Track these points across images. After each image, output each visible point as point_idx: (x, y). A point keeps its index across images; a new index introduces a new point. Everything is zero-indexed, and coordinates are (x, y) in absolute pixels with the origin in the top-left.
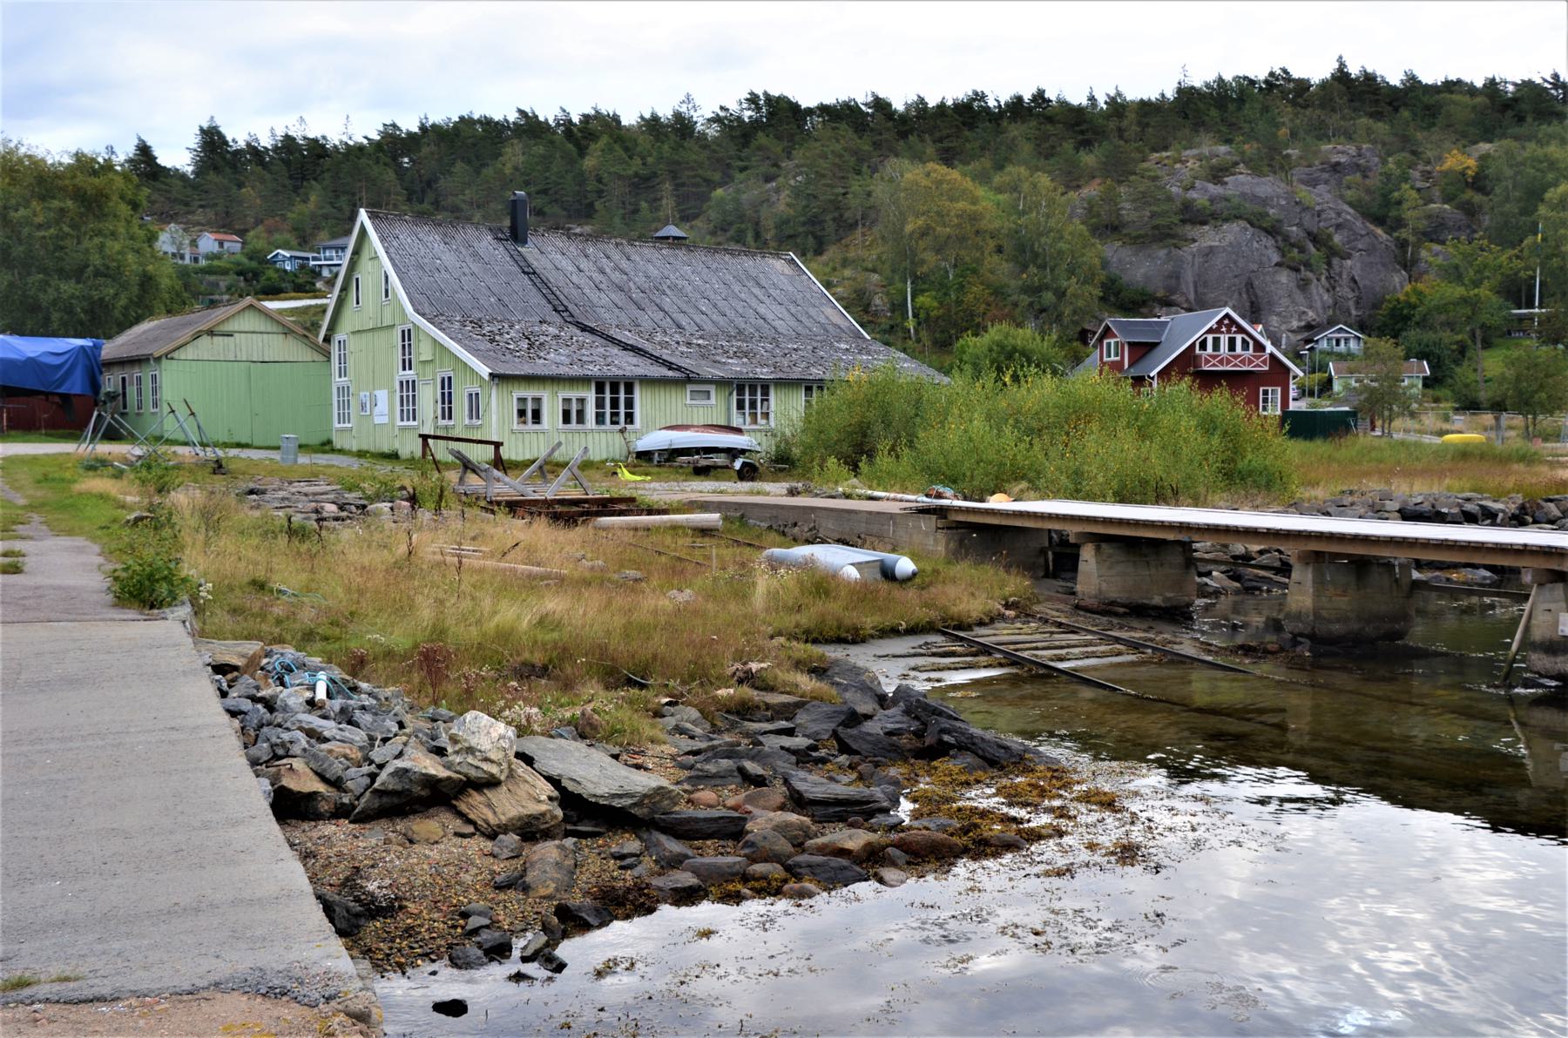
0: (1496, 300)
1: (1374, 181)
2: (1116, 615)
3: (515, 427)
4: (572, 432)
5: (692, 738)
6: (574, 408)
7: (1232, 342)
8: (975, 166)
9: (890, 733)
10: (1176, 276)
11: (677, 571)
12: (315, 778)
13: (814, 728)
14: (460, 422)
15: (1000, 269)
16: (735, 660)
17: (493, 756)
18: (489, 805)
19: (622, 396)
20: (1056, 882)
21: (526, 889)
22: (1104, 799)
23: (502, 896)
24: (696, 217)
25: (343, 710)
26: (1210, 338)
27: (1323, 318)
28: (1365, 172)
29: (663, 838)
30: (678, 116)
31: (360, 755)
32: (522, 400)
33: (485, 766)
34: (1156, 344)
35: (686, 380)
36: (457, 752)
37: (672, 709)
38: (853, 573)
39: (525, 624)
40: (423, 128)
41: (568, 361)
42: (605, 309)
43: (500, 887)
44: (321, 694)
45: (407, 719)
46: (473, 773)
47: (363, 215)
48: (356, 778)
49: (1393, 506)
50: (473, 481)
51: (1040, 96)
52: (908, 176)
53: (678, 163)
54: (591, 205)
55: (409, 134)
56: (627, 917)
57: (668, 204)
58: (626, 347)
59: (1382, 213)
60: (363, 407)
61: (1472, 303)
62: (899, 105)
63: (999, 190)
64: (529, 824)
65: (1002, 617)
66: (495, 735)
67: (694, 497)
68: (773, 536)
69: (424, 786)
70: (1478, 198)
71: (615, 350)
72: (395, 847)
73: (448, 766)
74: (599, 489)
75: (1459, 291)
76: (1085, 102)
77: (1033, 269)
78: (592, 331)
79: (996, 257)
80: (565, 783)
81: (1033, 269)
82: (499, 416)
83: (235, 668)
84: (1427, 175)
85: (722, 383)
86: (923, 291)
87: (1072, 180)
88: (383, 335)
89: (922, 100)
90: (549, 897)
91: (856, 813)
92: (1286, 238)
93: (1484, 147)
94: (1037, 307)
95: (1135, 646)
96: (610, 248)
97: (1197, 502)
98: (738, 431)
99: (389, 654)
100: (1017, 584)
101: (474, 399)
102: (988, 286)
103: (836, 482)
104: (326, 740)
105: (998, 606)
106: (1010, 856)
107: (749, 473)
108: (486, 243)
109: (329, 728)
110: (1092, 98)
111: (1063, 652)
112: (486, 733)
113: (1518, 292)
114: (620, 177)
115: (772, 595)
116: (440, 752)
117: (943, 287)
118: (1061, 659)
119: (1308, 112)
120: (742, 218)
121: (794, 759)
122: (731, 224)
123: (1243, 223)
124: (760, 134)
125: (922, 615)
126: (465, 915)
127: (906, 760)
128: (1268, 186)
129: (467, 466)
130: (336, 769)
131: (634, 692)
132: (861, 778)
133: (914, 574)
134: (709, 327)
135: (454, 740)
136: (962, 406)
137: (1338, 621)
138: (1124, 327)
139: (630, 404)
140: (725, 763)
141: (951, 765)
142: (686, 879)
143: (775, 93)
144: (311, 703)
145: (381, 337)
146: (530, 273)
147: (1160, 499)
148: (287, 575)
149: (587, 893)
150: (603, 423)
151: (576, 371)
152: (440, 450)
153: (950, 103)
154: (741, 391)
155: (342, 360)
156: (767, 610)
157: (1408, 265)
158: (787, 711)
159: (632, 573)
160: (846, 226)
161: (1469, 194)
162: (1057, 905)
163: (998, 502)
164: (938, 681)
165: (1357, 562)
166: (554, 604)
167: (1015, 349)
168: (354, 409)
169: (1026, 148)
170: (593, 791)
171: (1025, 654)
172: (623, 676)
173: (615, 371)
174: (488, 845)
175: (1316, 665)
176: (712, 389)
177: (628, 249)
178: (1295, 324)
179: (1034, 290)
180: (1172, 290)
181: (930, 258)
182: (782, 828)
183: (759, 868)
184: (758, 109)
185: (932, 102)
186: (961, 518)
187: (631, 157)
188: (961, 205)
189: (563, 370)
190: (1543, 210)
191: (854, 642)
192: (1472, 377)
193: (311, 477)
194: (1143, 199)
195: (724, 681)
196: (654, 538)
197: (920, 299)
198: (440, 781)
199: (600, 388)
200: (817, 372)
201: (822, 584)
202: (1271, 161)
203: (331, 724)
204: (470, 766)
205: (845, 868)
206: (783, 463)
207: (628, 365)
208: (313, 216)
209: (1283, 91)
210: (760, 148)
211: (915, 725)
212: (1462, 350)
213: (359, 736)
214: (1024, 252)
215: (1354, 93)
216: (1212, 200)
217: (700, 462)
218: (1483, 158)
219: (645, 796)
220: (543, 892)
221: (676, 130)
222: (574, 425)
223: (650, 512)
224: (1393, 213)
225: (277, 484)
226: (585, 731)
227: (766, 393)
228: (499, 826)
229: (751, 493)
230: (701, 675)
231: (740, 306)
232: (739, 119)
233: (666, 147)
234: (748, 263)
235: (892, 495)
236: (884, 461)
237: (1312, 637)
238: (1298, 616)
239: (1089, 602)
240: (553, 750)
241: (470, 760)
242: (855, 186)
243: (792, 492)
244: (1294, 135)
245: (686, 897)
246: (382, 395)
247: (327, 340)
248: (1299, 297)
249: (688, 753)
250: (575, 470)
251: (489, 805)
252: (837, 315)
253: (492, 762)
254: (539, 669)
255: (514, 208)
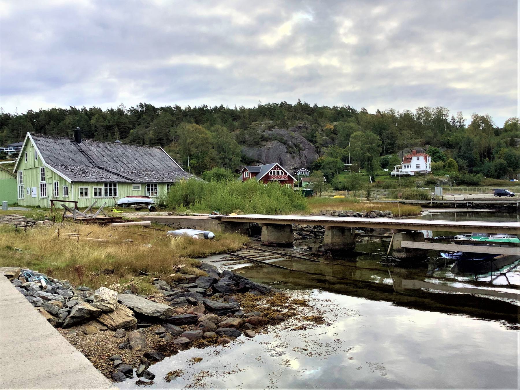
0: (341, 162)
1: (309, 131)
2: (274, 246)
3: (79, 197)
4: (97, 198)
5: (167, 290)
6: (98, 191)
7: (278, 172)
8: (205, 125)
9: (227, 285)
10: (260, 155)
11: (144, 239)
12: (48, 314)
13: (203, 285)
14: (61, 195)
15: (213, 153)
16: (174, 265)
17: (111, 302)
18: (112, 319)
19: (113, 188)
20: (302, 332)
21: (131, 348)
22: (301, 302)
23: (123, 352)
24: (125, 138)
25: (53, 289)
26: (273, 171)
27: (298, 166)
28: (307, 128)
29: (172, 326)
30: (119, 109)
31: (62, 304)
32: (82, 189)
33: (109, 306)
34: (258, 173)
35: (132, 183)
36: (98, 301)
37: (157, 282)
38: (197, 237)
39: (103, 256)
40: (40, 111)
41: (95, 177)
42: (105, 161)
43: (121, 348)
44: (44, 284)
45: (74, 291)
46: (104, 308)
47: (28, 134)
48: (63, 312)
49: (337, 214)
50: (68, 214)
51: (222, 107)
52: (187, 127)
53: (119, 122)
54: (93, 134)
55: (36, 113)
56: (169, 356)
57: (117, 134)
58: (113, 173)
59: (312, 139)
60: (28, 192)
61: (336, 162)
62: (183, 108)
63: (212, 132)
64: (126, 325)
65: (243, 248)
66: (111, 295)
67: (140, 216)
68: (166, 227)
69: (88, 314)
70: (335, 136)
71: (110, 174)
72: (81, 337)
73: (93, 306)
74: (109, 215)
75: (332, 159)
76: (234, 109)
77: (222, 153)
78: (102, 169)
79: (212, 150)
80: (135, 309)
81: (222, 153)
82: (74, 193)
83: (12, 276)
84: (322, 130)
85: (142, 183)
86: (192, 159)
87: (232, 129)
88: (35, 170)
89: (189, 107)
90: (140, 350)
91: (229, 312)
92: (288, 145)
93: (335, 123)
94: (224, 163)
95: (284, 255)
96: (106, 145)
97: (287, 214)
98: (148, 197)
99: (57, 269)
100: (245, 239)
101: (66, 189)
102: (210, 158)
103: (183, 211)
104: (50, 300)
105: (241, 245)
106: (282, 323)
107: (153, 209)
108: (68, 143)
109: (49, 295)
110: (236, 108)
111: (264, 258)
112: (107, 294)
113: (345, 160)
114: (102, 126)
115: (178, 245)
116: (89, 301)
117: (198, 158)
118: (264, 260)
119: (292, 113)
120: (139, 138)
121: (202, 295)
122: (136, 140)
123: (277, 141)
124: (144, 115)
125: (222, 249)
126: (113, 360)
127: (235, 294)
128: (283, 132)
129: (66, 209)
130: (56, 309)
131: (144, 276)
132: (225, 300)
133: (214, 237)
134: (137, 168)
135: (96, 297)
136: (225, 188)
137: (338, 246)
138: (249, 168)
139: (115, 190)
140: (183, 298)
141: (250, 294)
142: (185, 340)
143: (148, 103)
144: (41, 287)
145: (34, 171)
146: (82, 151)
147: (276, 213)
148: (18, 245)
149: (152, 348)
150: (107, 195)
151: (98, 180)
152: (58, 205)
153: (197, 108)
154: (148, 186)
155: (21, 178)
156: (177, 249)
157: (318, 153)
158: (192, 280)
159: (130, 240)
160: (169, 141)
161: (332, 135)
162: (306, 340)
163: (233, 215)
164: (232, 268)
165: (341, 229)
166: (111, 250)
167: (220, 175)
168: (25, 193)
169: (219, 120)
170: (146, 311)
171: (254, 259)
172: (140, 272)
173: (110, 180)
174: (114, 333)
175: (333, 259)
176: (140, 185)
177: (112, 145)
178: (292, 168)
179: (223, 159)
180: (259, 159)
181: (194, 150)
182: (210, 319)
183: (208, 334)
184: (143, 108)
185: (192, 108)
186: (225, 220)
187: (105, 120)
188: (202, 135)
189: (94, 180)
190: (351, 139)
191: (203, 258)
192: (336, 182)
193: (14, 214)
194: (251, 134)
195: (172, 272)
196: (132, 229)
197: (192, 161)
198: (94, 312)
199: (106, 186)
200: (170, 180)
201: (190, 241)
202: (284, 125)
203: (50, 294)
204: (103, 306)
205: (234, 331)
206: (162, 206)
207: (114, 178)
208: (5, 137)
209: (285, 106)
210: (144, 119)
211: (234, 282)
212: (333, 174)
213: (61, 298)
214: (220, 149)
215: (303, 109)
216: (269, 135)
217: (138, 207)
218: (335, 126)
219: (164, 312)
220: (137, 349)
221: (118, 113)
222: (98, 196)
223: (128, 221)
224: (314, 139)
225: (3, 216)
226: (134, 291)
227: (156, 186)
228: (116, 326)
229: (157, 215)
230: (164, 270)
231: (146, 162)
232: (137, 110)
233: (116, 118)
234: (148, 149)
235: (201, 214)
236: (197, 205)
237: (331, 250)
238: (327, 245)
239: (265, 243)
240: (128, 298)
241: (103, 304)
242: (172, 130)
243: (169, 214)
244: (288, 119)
245: (186, 346)
246: (35, 189)
247: (16, 172)
248: (292, 160)
249: (168, 296)
250: (102, 209)
251: (112, 319)
252: (174, 164)
253: (111, 304)
254: (114, 271)
255: (76, 132)
